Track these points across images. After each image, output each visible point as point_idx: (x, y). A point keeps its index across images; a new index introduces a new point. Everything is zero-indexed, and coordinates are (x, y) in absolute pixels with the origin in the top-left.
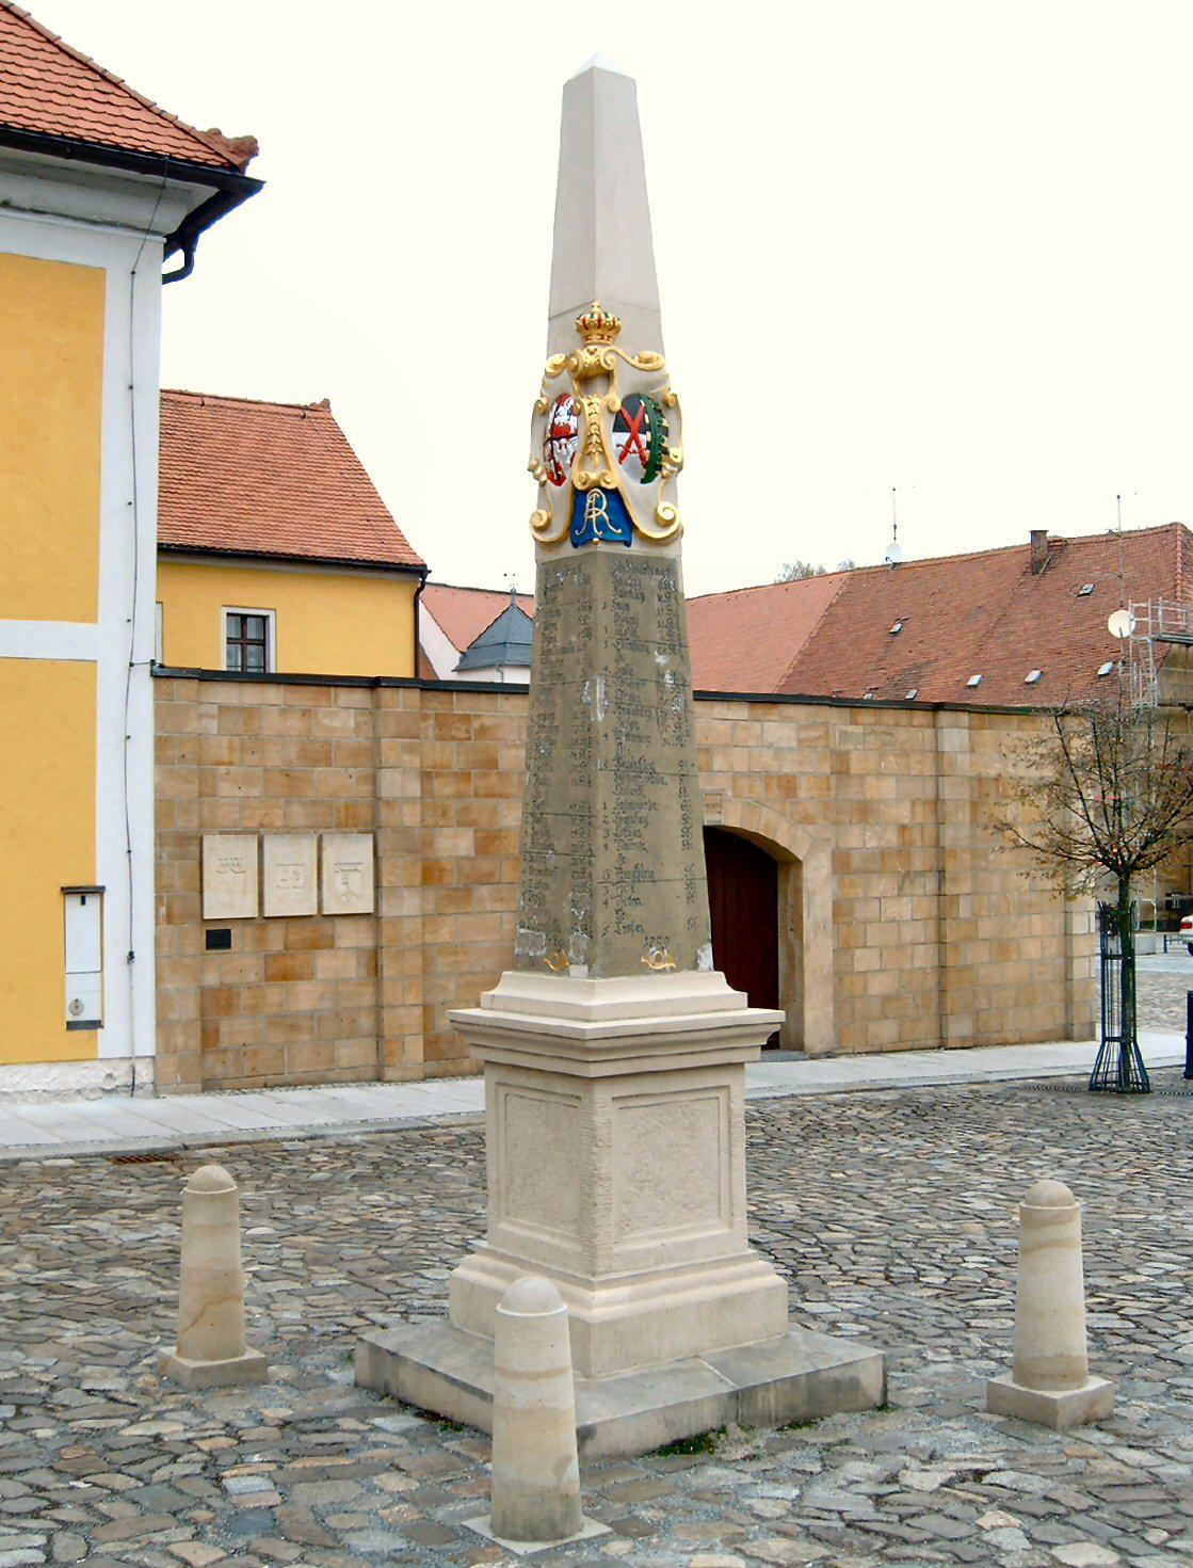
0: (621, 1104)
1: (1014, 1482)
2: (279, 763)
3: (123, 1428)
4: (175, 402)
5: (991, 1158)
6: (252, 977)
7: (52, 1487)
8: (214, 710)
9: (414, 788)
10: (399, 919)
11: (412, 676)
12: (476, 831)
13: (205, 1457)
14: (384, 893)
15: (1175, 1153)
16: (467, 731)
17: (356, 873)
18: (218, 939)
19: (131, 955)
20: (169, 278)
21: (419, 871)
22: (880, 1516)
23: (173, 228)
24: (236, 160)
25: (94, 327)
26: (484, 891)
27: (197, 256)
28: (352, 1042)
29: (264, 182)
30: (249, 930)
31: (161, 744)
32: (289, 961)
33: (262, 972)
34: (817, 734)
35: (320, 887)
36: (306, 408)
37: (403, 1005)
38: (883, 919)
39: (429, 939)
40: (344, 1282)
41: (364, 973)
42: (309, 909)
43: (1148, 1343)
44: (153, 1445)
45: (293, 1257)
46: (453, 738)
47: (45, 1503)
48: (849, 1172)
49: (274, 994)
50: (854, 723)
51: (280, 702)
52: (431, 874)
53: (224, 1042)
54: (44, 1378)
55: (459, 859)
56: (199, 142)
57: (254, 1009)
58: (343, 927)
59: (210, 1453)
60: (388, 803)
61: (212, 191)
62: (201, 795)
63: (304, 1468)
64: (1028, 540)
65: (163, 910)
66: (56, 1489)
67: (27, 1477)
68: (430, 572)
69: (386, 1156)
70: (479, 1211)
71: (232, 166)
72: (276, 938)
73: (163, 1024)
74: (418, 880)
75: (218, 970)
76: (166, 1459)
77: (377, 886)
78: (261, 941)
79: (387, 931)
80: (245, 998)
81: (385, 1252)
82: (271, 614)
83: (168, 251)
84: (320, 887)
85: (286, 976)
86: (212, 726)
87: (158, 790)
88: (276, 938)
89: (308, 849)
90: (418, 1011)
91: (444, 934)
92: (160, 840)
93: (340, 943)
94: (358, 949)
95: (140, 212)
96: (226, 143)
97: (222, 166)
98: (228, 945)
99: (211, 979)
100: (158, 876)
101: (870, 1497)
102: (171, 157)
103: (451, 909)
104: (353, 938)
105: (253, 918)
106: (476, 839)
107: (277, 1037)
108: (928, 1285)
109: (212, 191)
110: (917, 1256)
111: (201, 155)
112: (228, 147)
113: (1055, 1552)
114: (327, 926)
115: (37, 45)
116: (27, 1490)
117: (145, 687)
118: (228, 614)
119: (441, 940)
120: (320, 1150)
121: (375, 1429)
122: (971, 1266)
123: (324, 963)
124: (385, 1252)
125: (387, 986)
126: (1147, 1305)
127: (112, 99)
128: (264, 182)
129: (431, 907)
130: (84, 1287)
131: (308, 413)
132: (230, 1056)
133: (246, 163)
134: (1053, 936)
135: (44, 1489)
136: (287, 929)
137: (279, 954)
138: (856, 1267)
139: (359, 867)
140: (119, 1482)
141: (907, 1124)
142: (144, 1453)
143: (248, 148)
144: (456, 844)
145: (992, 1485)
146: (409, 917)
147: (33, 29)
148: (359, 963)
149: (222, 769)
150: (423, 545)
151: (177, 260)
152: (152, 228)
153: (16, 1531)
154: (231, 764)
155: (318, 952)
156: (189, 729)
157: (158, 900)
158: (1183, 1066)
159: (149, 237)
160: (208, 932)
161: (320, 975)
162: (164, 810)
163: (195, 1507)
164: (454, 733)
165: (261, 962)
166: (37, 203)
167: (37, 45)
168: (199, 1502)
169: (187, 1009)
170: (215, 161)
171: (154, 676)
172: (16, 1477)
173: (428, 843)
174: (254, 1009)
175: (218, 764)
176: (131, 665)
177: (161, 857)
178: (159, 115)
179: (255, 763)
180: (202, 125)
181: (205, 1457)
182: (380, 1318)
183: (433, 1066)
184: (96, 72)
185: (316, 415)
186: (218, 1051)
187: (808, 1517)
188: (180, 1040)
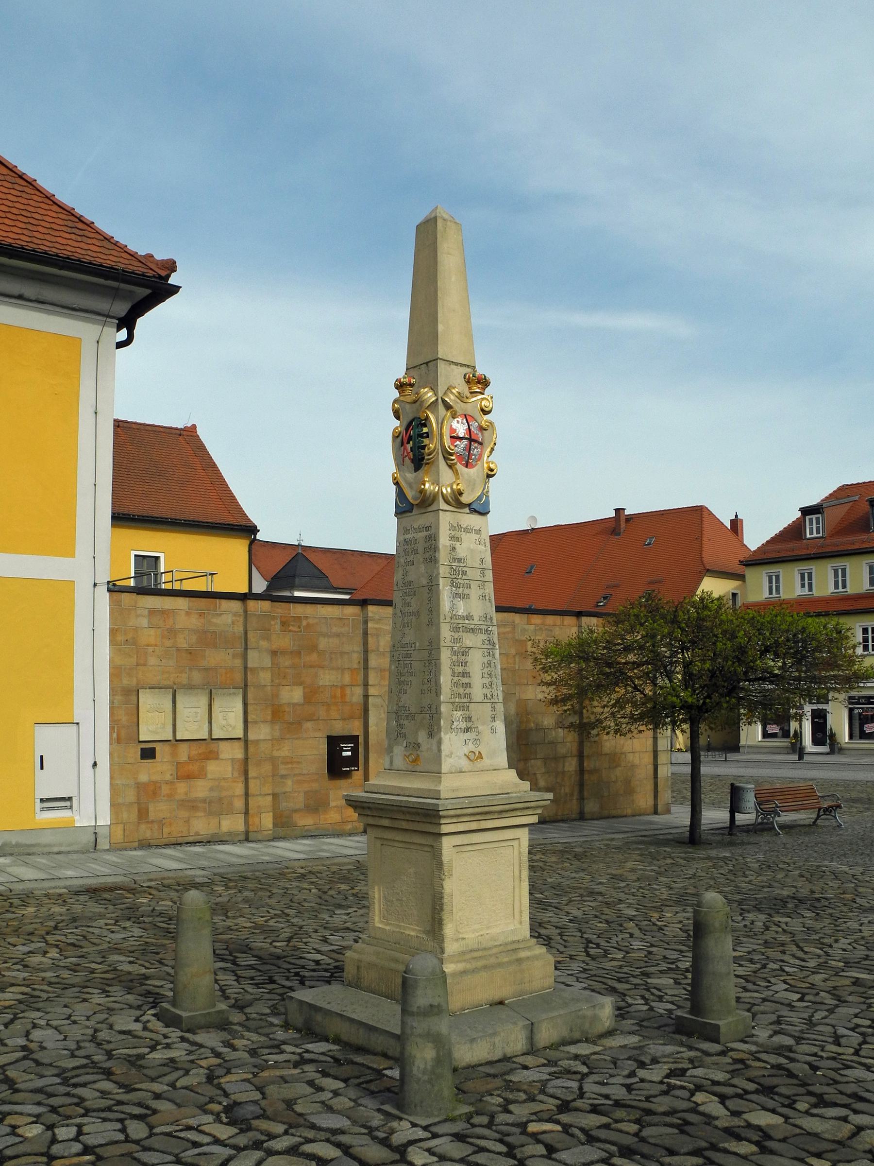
0: (459, 849)
1: (706, 1074)
2: (185, 645)
3: (148, 1054)
4: (119, 425)
5: (628, 885)
6: (168, 777)
7: (115, 1092)
8: (146, 612)
9: (267, 662)
10: (257, 742)
11: (247, 591)
12: (304, 688)
13: (206, 1071)
14: (250, 725)
15: (736, 879)
16: (299, 627)
17: (232, 713)
18: (148, 754)
19: (95, 764)
20: (120, 345)
21: (269, 712)
22: (633, 1097)
23: (123, 314)
24: (163, 273)
25: (74, 376)
26: (309, 725)
27: (136, 332)
28: (228, 816)
29: (181, 287)
30: (166, 748)
31: (113, 632)
32: (191, 767)
33: (175, 773)
34: (508, 630)
35: (210, 723)
36: (181, 429)
37: (260, 795)
38: (546, 741)
39: (276, 754)
40: (257, 962)
41: (236, 774)
42: (205, 735)
43: (757, 991)
44: (170, 1064)
45: (221, 947)
46: (290, 631)
47: (112, 1102)
48: (546, 893)
49: (182, 788)
50: (529, 623)
51: (186, 608)
52: (277, 714)
53: (152, 816)
54: (88, 1023)
55: (295, 705)
56: (140, 262)
57: (170, 797)
58: (223, 745)
59: (208, 1069)
60: (251, 669)
61: (148, 291)
62: (137, 665)
63: (270, 1076)
64: (613, 514)
65: (115, 735)
66: (117, 1094)
67: (97, 1086)
68: (259, 531)
69: (260, 886)
70: (327, 919)
71: (160, 277)
72: (184, 752)
73: (115, 806)
74: (269, 718)
75: (147, 772)
76: (181, 1072)
77: (246, 721)
78: (174, 754)
79: (251, 749)
80: (165, 790)
81: (278, 944)
82: (162, 555)
83: (119, 329)
84: (210, 723)
85: (189, 777)
86: (145, 622)
87: (111, 661)
88: (184, 752)
89: (204, 701)
90: (270, 798)
91: (284, 751)
92: (113, 691)
93: (222, 756)
94: (233, 760)
95: (103, 305)
96: (157, 263)
97: (154, 276)
98: (154, 757)
99: (143, 778)
100: (112, 714)
101: (622, 1085)
102: (123, 271)
103: (288, 736)
104: (234, 752)
105: (170, 741)
106: (304, 693)
107: (184, 814)
108: (613, 959)
109: (148, 291)
110: (603, 943)
111: (141, 270)
112: (157, 264)
113: (745, 1116)
114: (213, 746)
115: (40, 199)
116: (98, 1094)
117: (103, 596)
118: (135, 555)
119: (283, 754)
120: (219, 883)
121: (307, 1051)
122: (635, 947)
123: (212, 768)
124: (278, 944)
125: (252, 784)
126: (749, 969)
127: (86, 233)
128: (181, 287)
129: (277, 734)
130: (96, 968)
131: (184, 433)
132: (156, 826)
133: (168, 276)
134: (646, 752)
135: (109, 1093)
136: (190, 747)
137: (185, 763)
138: (567, 949)
139: (234, 710)
140: (157, 1087)
141: (571, 865)
142: (166, 1069)
143: (171, 266)
144: (294, 695)
145: (691, 1076)
146: (264, 740)
147: (38, 190)
148: (233, 768)
149: (151, 649)
150: (254, 513)
151: (123, 335)
152: (111, 314)
153: (100, 1120)
154: (156, 645)
155: (208, 762)
156: (131, 624)
157: (112, 728)
158: (727, 828)
159: (109, 320)
160: (142, 749)
161: (209, 776)
162: (115, 673)
163: (210, 1102)
164: (291, 628)
165: (174, 768)
166: (40, 297)
167: (40, 199)
168: (212, 1100)
169: (130, 796)
170: (151, 273)
171: (109, 590)
172: (89, 1086)
173: (276, 696)
174: (170, 797)
175: (148, 645)
176: (95, 585)
177: (113, 702)
178: (115, 245)
179: (171, 645)
180: (142, 252)
181: (206, 1071)
182: (288, 984)
183: (281, 832)
184: (76, 217)
185: (189, 433)
186: (148, 822)
187: (590, 1099)
188: (125, 815)
